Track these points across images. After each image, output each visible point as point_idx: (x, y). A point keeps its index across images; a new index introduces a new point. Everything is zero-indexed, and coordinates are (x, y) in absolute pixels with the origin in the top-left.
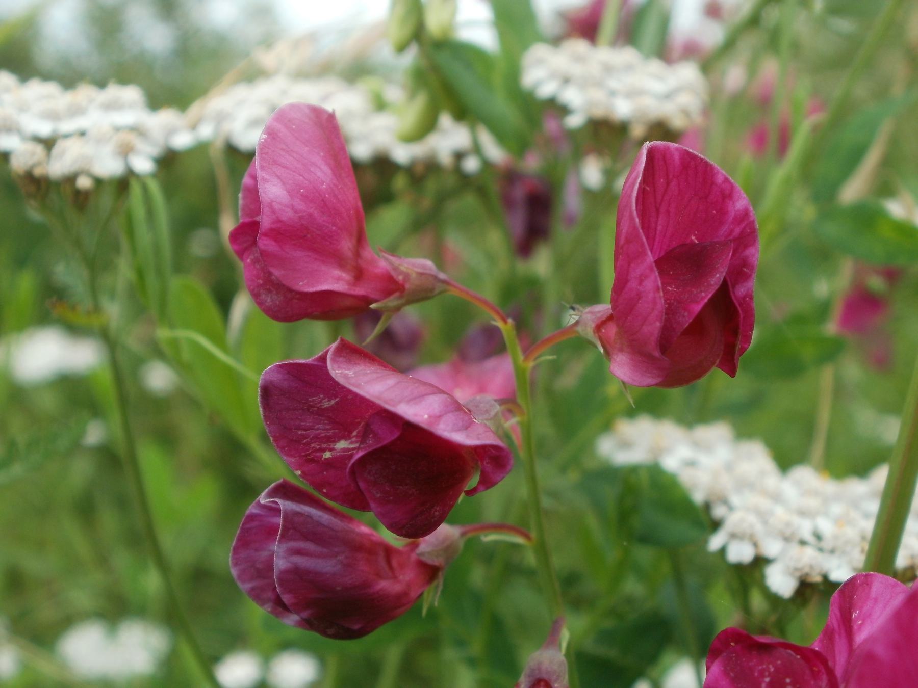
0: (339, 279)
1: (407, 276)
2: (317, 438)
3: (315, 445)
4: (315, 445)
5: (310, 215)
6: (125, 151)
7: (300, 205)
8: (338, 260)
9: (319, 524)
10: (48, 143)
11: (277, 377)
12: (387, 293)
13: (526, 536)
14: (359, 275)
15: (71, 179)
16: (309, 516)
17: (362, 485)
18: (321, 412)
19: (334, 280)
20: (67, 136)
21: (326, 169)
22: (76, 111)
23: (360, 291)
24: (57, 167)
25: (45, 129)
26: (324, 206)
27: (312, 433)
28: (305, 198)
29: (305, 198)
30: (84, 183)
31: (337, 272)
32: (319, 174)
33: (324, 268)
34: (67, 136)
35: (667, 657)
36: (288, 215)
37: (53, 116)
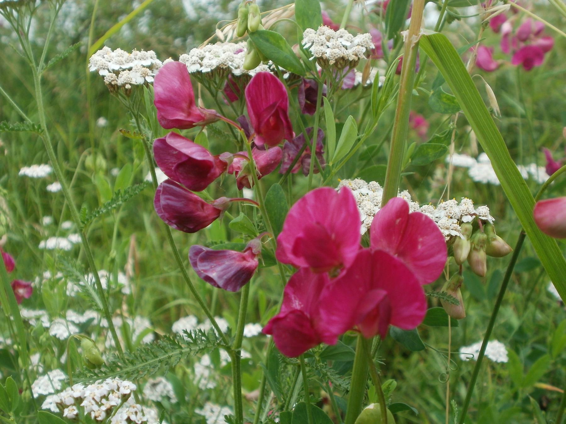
0: (181, 116)
1: (205, 115)
2: (171, 163)
3: (171, 165)
4: (171, 165)
5: (170, 96)
6: (144, 75)
7: (167, 93)
8: (182, 110)
9: (175, 191)
10: (117, 73)
11: (158, 144)
12: (199, 120)
13: (257, 204)
14: (189, 114)
15: (124, 85)
16: (172, 188)
17: (178, 174)
18: (173, 155)
19: (181, 116)
20: (124, 70)
21: (178, 83)
22: (129, 61)
23: (190, 119)
24: (120, 82)
25: (117, 67)
26: (176, 93)
27: (170, 161)
28: (169, 91)
29: (169, 91)
30: (128, 87)
31: (181, 113)
32: (175, 84)
33: (177, 112)
34: (124, 70)
35: (509, 360)
36: (163, 96)
37: (121, 63)
